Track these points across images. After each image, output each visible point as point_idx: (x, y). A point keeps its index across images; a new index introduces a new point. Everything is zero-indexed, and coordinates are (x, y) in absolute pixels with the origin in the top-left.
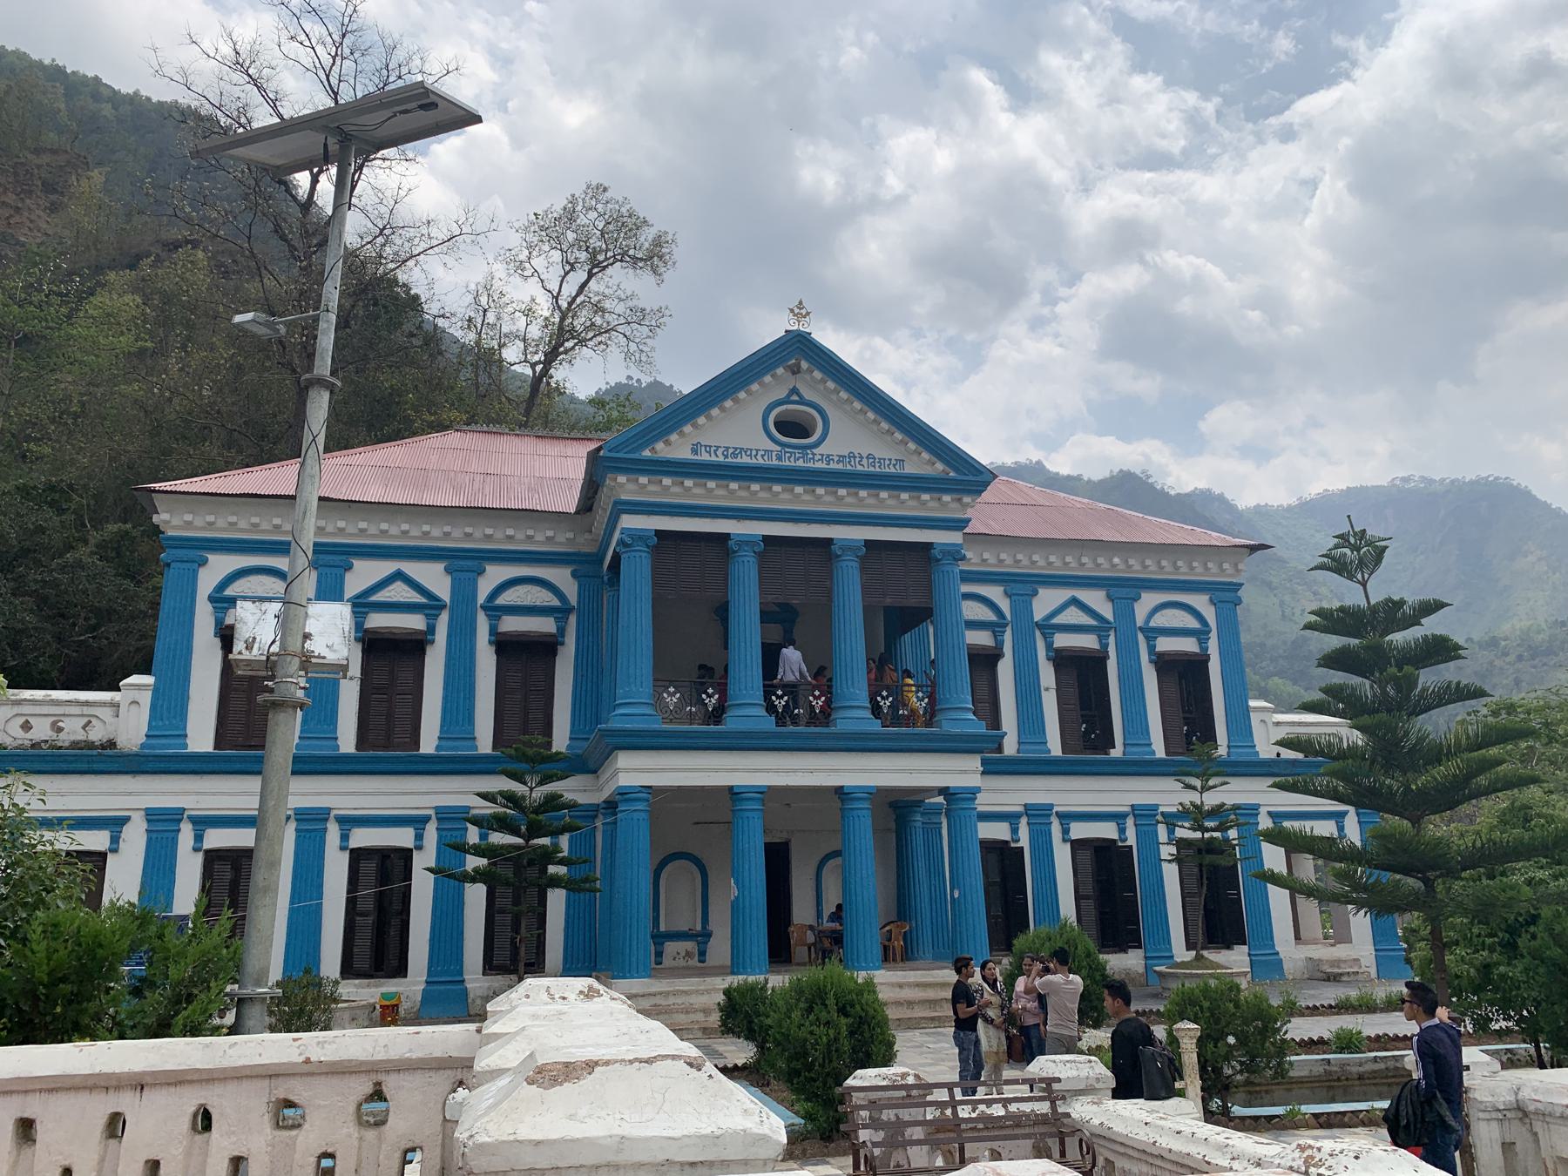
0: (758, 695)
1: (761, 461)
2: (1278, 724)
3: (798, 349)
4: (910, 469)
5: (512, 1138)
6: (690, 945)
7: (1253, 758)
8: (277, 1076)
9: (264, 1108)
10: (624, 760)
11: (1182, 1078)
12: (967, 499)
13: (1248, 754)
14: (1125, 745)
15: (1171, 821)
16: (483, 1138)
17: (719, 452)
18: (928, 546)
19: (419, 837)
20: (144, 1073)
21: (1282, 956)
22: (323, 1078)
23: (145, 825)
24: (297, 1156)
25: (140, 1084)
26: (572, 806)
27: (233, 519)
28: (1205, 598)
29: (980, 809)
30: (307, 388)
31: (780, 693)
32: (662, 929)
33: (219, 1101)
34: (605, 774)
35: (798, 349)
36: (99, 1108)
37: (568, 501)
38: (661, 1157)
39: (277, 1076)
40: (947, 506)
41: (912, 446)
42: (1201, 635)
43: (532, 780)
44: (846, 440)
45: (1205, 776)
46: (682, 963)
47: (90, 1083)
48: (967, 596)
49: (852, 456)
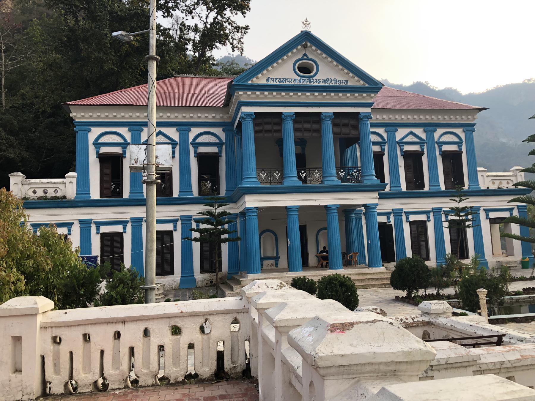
0: (295, 173)
1: (293, 83)
2: (488, 176)
3: (306, 39)
4: (350, 84)
5: (332, 354)
6: (272, 261)
7: (478, 189)
8: (171, 317)
9: (167, 328)
10: (247, 198)
11: (480, 309)
12: (373, 95)
13: (476, 188)
14: (430, 186)
15: (447, 213)
16: (321, 354)
17: (277, 81)
18: (320, 114)
19: (175, 227)
20: (125, 317)
21: (487, 261)
22: (187, 318)
23: (79, 225)
24: (181, 345)
25: (124, 321)
26: (229, 214)
27: (99, 114)
28: (421, 130)
29: (378, 211)
30: (147, 61)
31: (303, 172)
32: (262, 256)
33: (152, 326)
34: (240, 203)
35: (306, 39)
36: (111, 330)
37: (220, 103)
38: (390, 360)
39: (171, 317)
40: (365, 98)
41: (351, 75)
42: (219, 145)
43: (216, 206)
44: (325, 74)
45: (459, 196)
46: (270, 268)
47: (107, 321)
48: (373, 133)
49: (328, 80)
